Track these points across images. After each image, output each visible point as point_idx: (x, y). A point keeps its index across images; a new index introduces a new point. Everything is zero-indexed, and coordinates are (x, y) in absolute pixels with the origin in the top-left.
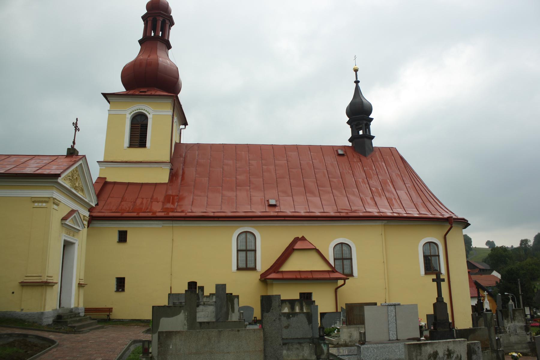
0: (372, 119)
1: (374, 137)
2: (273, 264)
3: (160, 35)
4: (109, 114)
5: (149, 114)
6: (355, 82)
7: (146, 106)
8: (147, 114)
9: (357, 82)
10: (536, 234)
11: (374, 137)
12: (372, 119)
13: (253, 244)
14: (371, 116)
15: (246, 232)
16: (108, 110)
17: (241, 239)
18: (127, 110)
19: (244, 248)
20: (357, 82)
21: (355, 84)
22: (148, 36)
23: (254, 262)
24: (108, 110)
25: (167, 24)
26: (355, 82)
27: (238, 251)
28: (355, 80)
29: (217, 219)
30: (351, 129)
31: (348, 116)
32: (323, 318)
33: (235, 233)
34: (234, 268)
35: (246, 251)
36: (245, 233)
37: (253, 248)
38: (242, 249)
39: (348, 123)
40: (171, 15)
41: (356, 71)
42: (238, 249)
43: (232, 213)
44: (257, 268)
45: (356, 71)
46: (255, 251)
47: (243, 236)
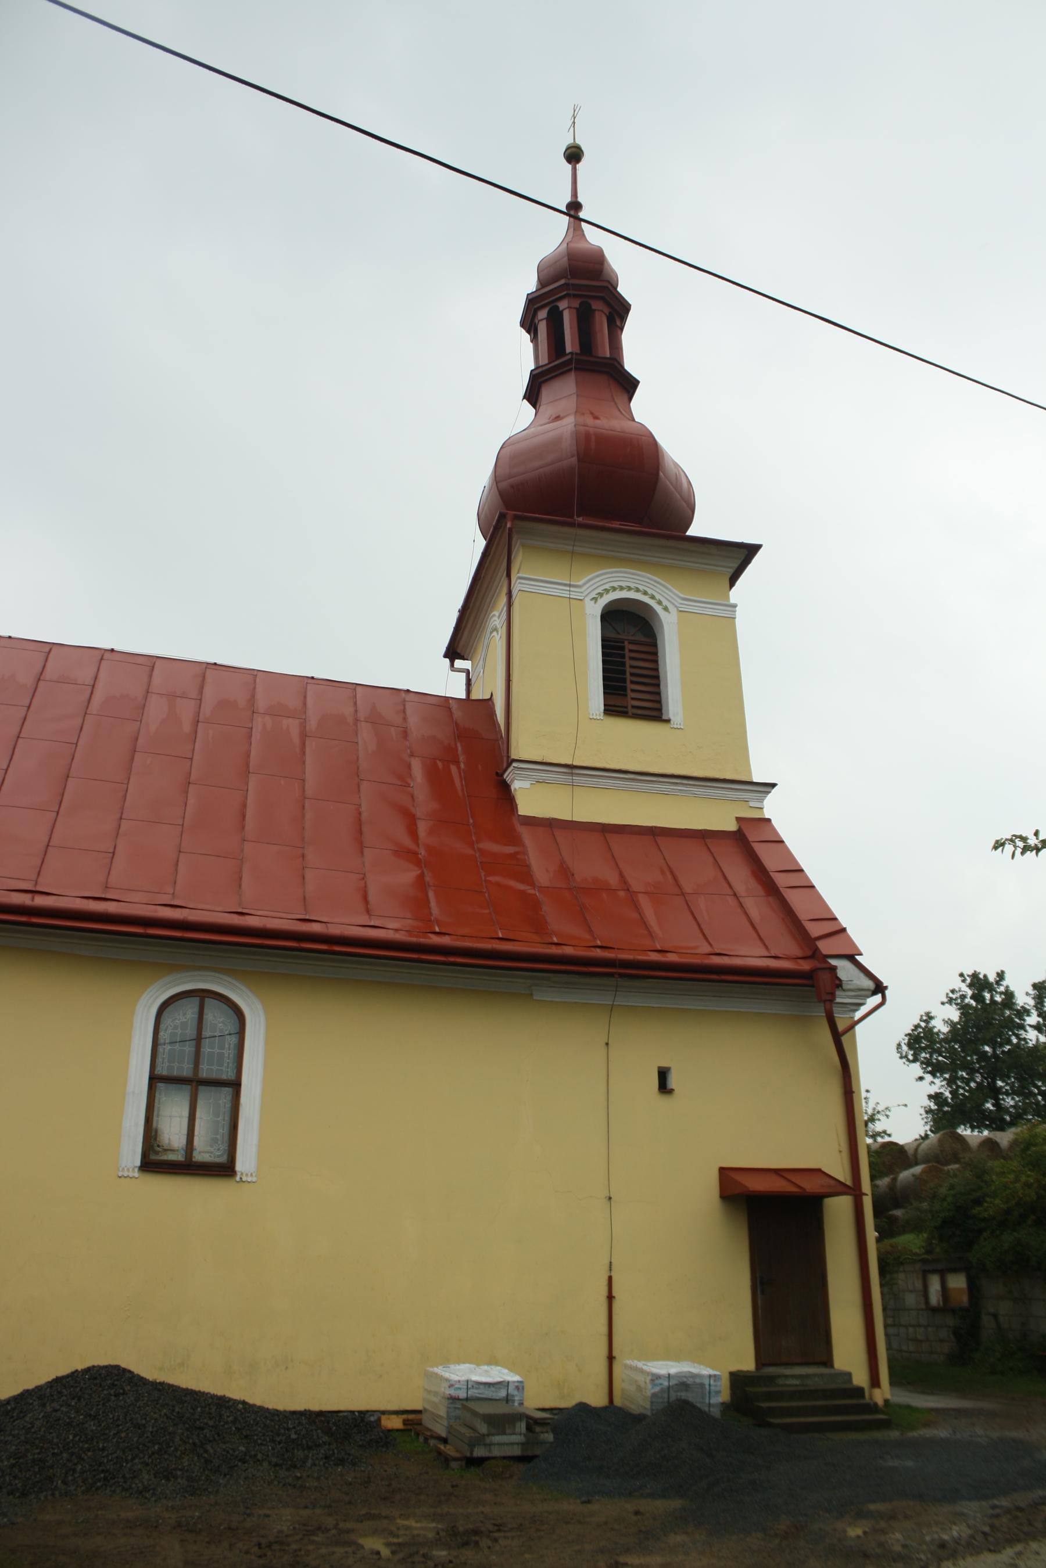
1: (750, 551)
5: (666, 609)
7: (674, 590)
8: (658, 609)
11: (750, 551)
13: (229, 1053)
15: (203, 995)
17: (176, 1027)
18: (585, 584)
19: (186, 1070)
23: (226, 1138)
25: (597, 314)
27: (154, 1079)
29: (24, 919)
32: (928, 1111)
33: (149, 990)
34: (132, 1152)
35: (617, 986)
36: (196, 1001)
37: (229, 1074)
38: (175, 1073)
42: (159, 1071)
43: (85, 901)
44: (239, 1167)
46: (235, 1085)
47: (187, 1013)
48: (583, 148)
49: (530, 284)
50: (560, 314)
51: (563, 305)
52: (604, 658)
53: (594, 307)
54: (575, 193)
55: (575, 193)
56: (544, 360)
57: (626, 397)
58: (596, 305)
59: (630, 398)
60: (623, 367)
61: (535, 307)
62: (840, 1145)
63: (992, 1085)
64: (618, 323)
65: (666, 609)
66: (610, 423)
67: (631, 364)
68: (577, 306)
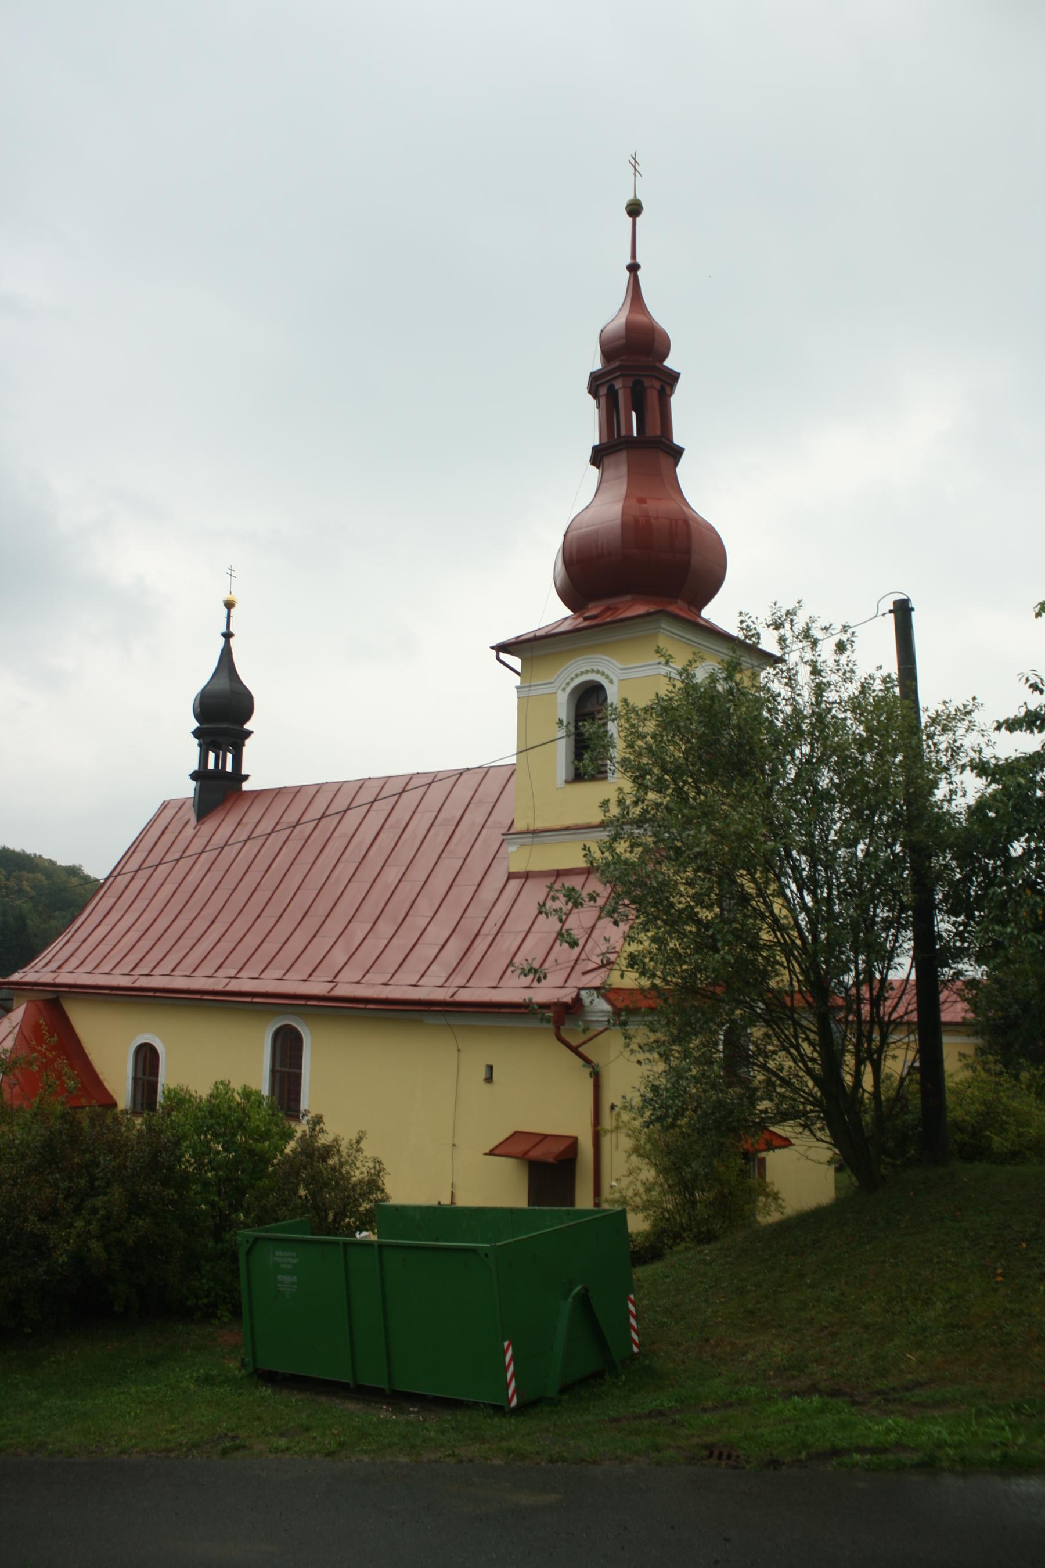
0: (249, 733)
2: (98, 1070)
3: (635, 434)
4: (518, 698)
5: (611, 682)
6: (224, 635)
9: (228, 635)
10: (192, 1089)
12: (249, 733)
14: (248, 726)
16: (517, 688)
20: (228, 635)
21: (223, 640)
22: (624, 437)
24: (517, 688)
26: (224, 635)
28: (224, 630)
30: (198, 749)
31: (198, 720)
39: (197, 733)
40: (668, 363)
41: (229, 605)
45: (229, 605)
48: (643, 205)
49: (595, 362)
50: (616, 392)
51: (618, 385)
52: (297, 1071)
53: (646, 385)
54: (634, 255)
55: (634, 255)
56: (605, 440)
57: (672, 460)
58: (647, 383)
59: (676, 464)
60: (672, 442)
61: (598, 383)
62: (659, 663)
63: (853, 991)
64: (668, 392)
65: (611, 682)
66: (657, 507)
67: (678, 440)
68: (631, 385)
